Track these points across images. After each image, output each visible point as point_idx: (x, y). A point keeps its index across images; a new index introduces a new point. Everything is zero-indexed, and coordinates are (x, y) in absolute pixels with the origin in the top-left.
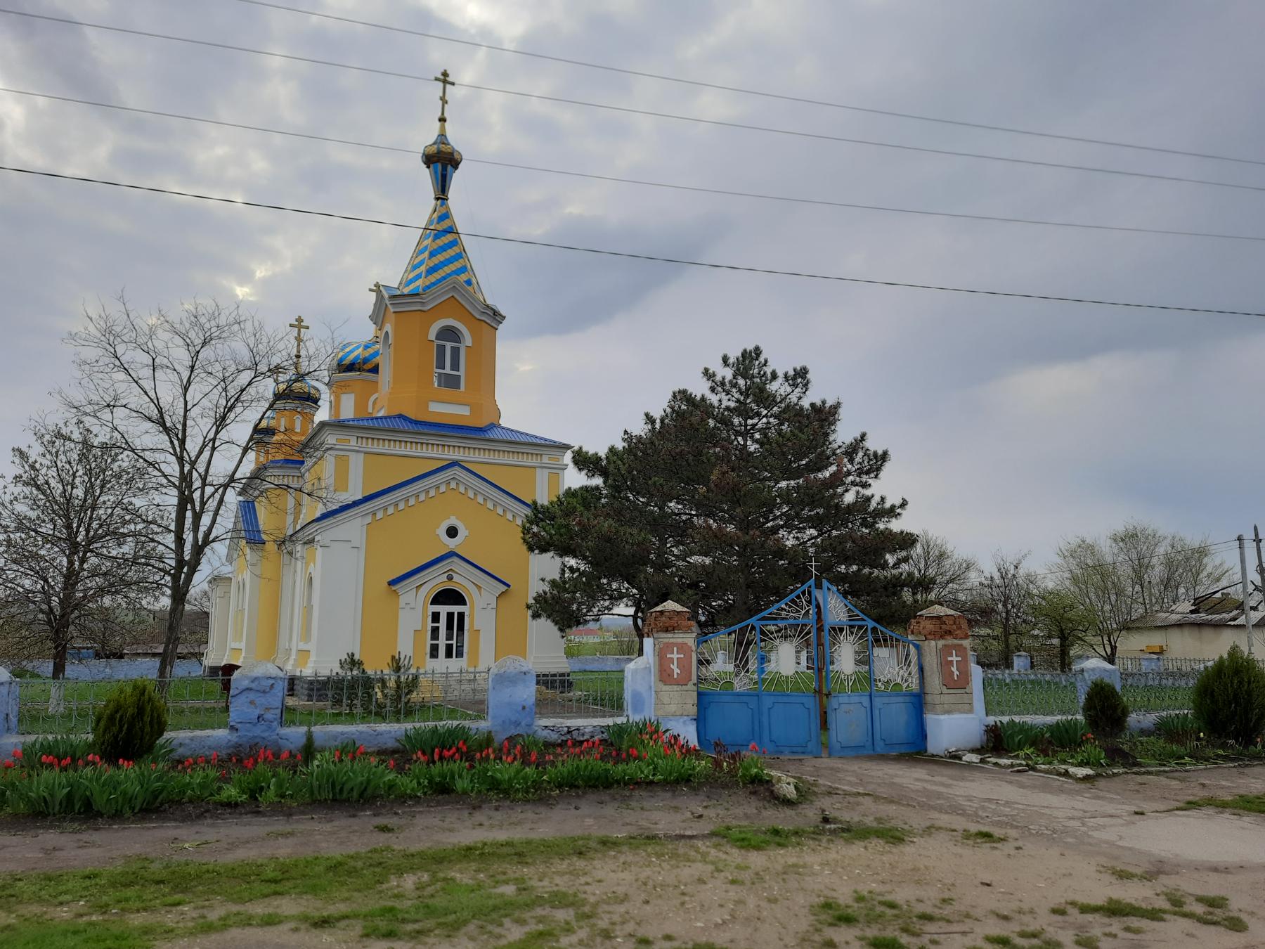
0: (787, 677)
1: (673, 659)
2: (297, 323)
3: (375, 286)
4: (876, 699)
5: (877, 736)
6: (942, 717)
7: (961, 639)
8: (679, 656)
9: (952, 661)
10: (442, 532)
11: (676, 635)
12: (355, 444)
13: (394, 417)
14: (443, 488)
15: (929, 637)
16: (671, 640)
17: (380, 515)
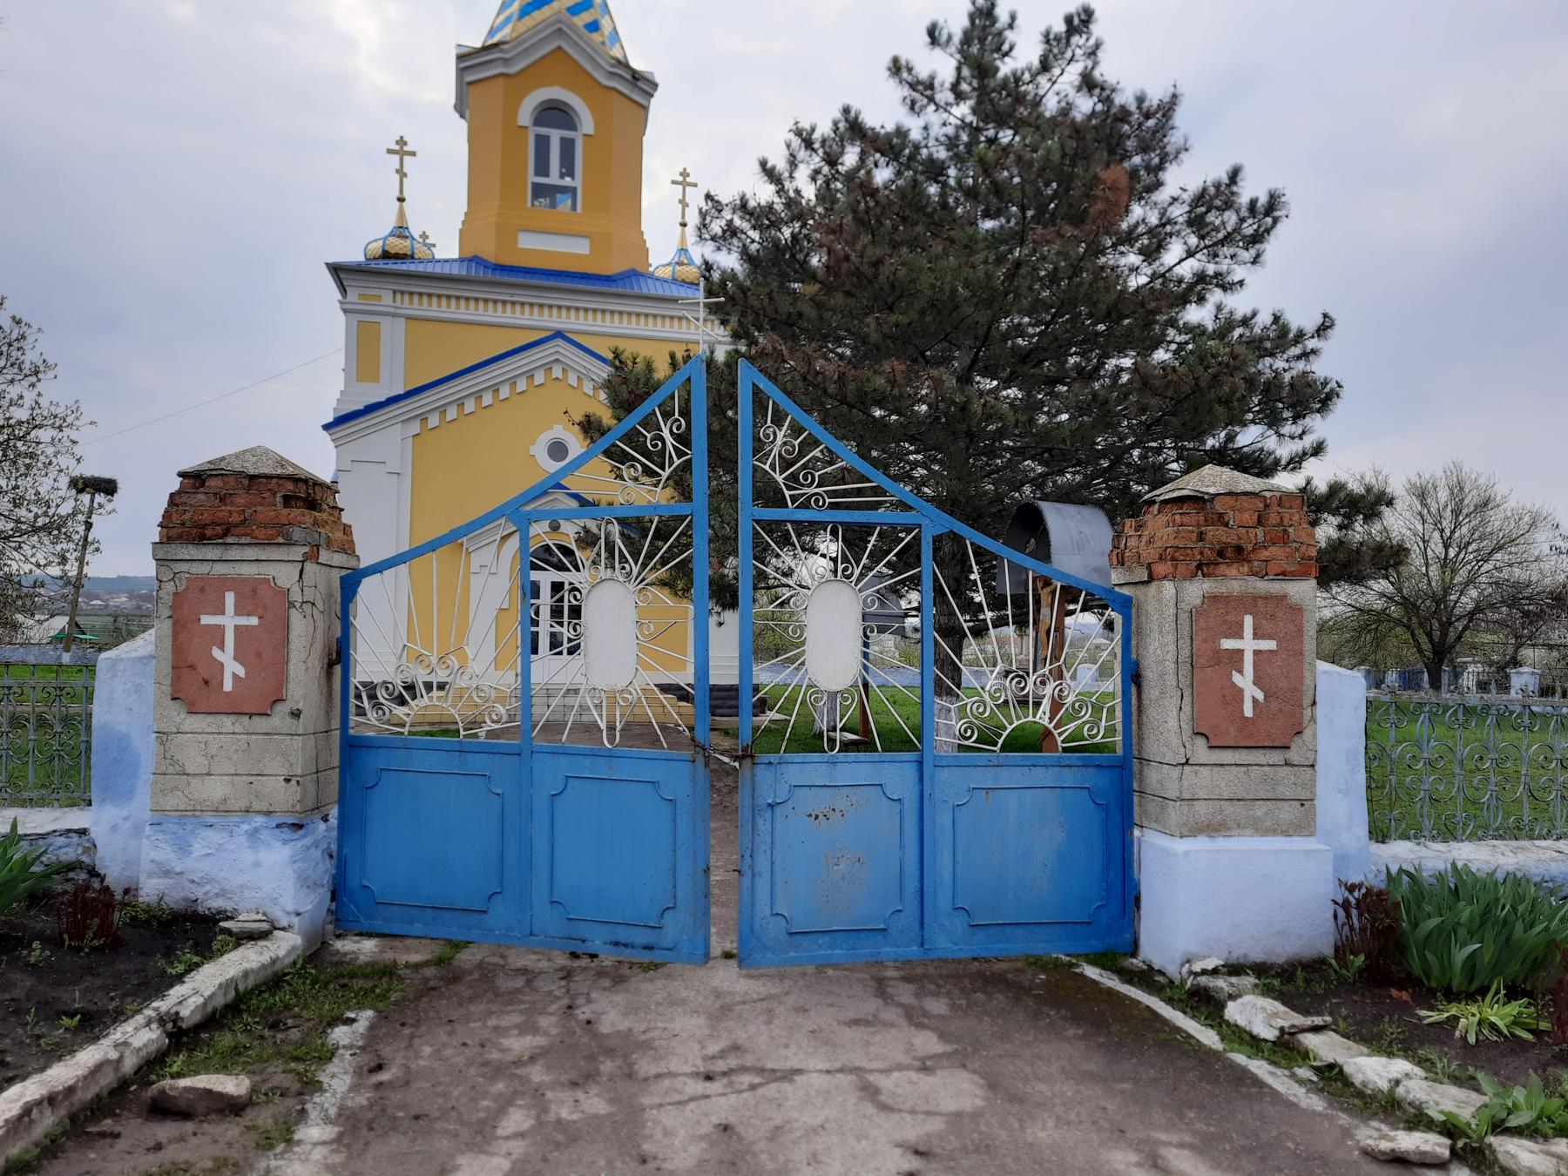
0: (833, 696)
1: (220, 630)
3: (681, 174)
4: (943, 775)
5: (941, 899)
6: (1181, 846)
7: (1284, 575)
8: (244, 621)
9: (1240, 652)
11: (234, 554)
12: (391, 303)
13: (470, 260)
14: (539, 378)
15: (1160, 569)
16: (220, 569)
17: (434, 421)
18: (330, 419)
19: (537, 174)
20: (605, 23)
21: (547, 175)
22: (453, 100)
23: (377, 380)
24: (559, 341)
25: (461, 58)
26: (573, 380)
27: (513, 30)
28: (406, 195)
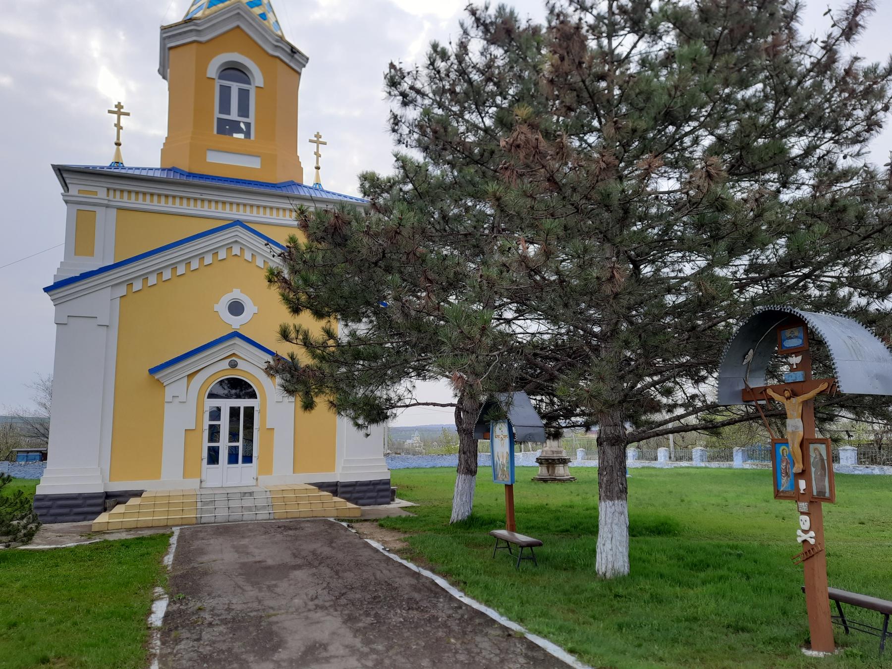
10: (222, 307)
13: (169, 170)
14: (222, 254)
17: (138, 285)
18: (51, 283)
19: (220, 112)
20: (270, 15)
21: (229, 114)
23: (92, 254)
24: (239, 228)
25: (164, 29)
26: (248, 256)
27: (203, 13)
28: (121, 141)
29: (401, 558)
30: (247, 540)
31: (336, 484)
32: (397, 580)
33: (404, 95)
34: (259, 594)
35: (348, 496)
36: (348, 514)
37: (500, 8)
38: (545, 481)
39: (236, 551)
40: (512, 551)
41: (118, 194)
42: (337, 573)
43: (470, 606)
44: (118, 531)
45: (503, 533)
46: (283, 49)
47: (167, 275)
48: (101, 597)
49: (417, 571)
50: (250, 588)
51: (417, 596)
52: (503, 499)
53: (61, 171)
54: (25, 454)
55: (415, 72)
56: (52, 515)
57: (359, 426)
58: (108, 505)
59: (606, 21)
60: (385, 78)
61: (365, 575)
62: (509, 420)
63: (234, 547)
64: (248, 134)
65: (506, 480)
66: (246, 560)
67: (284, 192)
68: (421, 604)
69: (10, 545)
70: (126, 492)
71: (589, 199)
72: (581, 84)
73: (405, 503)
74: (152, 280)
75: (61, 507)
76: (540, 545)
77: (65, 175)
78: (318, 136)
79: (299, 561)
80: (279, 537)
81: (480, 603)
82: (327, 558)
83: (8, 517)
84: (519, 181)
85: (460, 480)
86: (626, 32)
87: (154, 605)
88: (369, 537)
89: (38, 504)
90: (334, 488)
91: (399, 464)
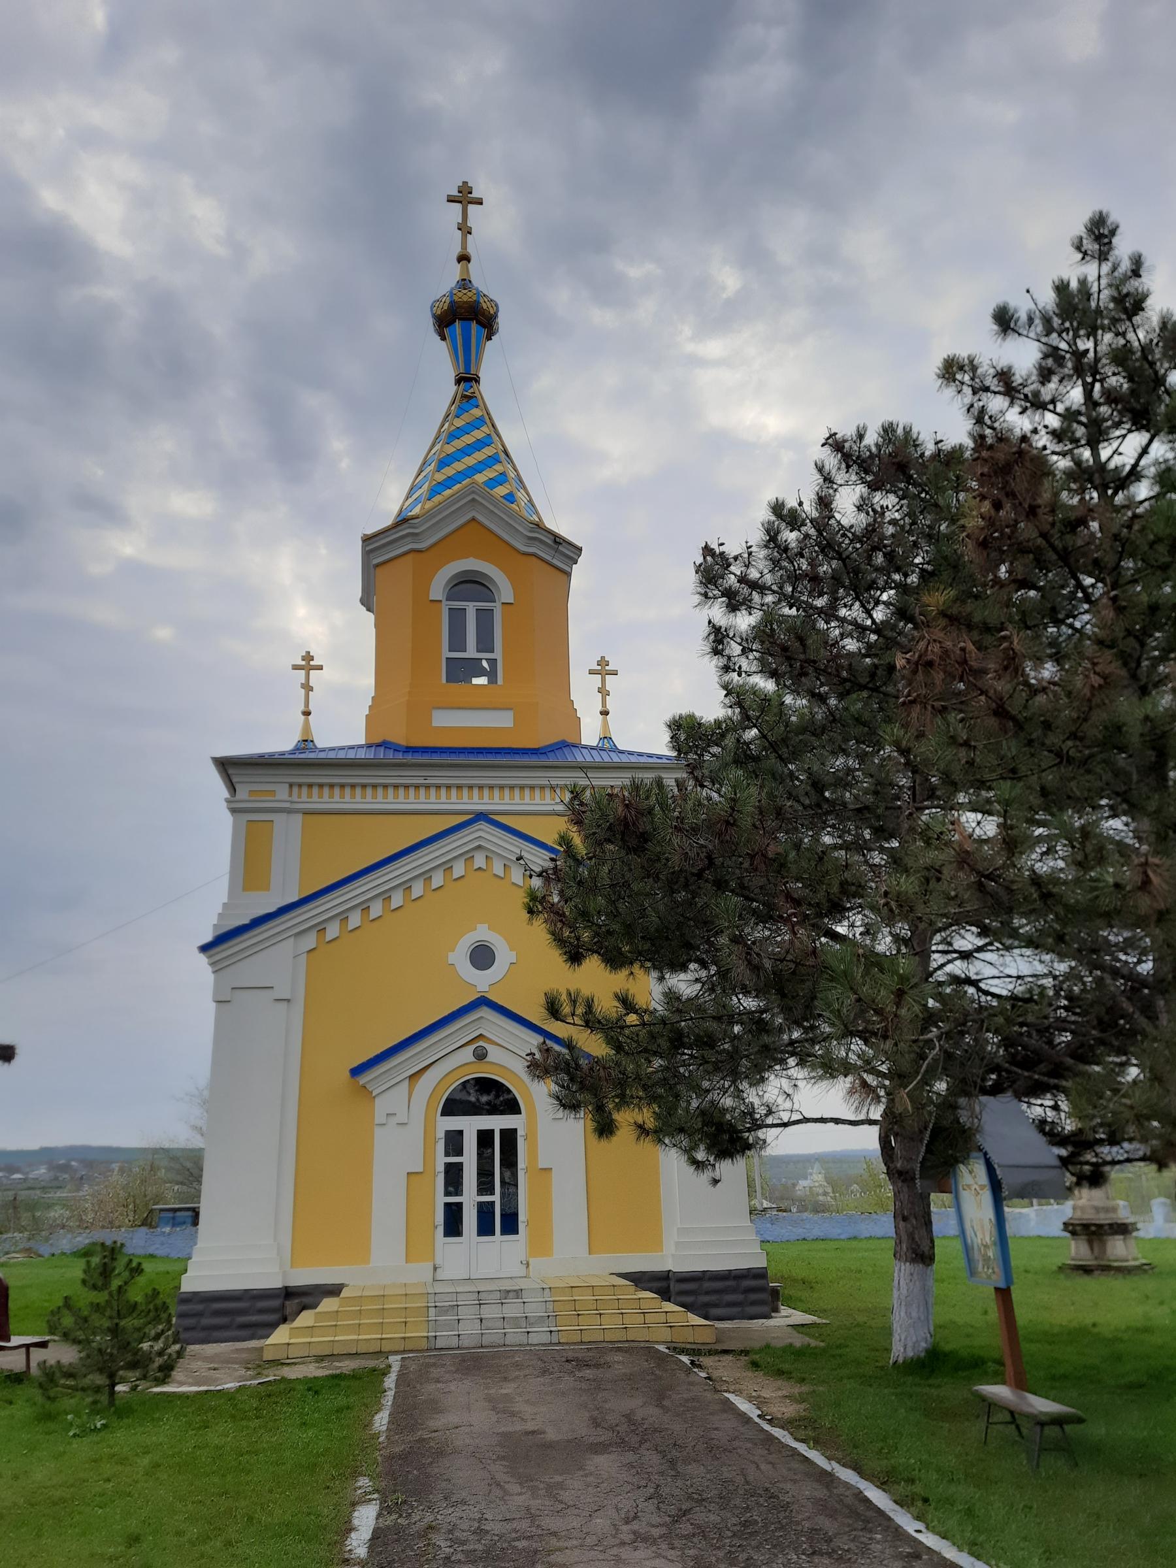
2: (303, 663)
10: (460, 957)
13: (379, 745)
17: (333, 931)
20: (520, 495)
22: (358, 593)
23: (267, 888)
24: (483, 825)
25: (367, 540)
26: (498, 869)
27: (423, 508)
29: (796, 1439)
30: (513, 1385)
31: (666, 1276)
32: (788, 1486)
33: (729, 594)
34: (531, 1502)
35: (689, 1299)
36: (690, 1337)
37: (885, 430)
38: (1086, 1270)
39: (494, 1408)
40: (1025, 1431)
41: (305, 790)
42: (673, 1463)
43: (938, 1554)
44: (303, 1360)
45: (1000, 1391)
46: (541, 541)
47: (376, 909)
48: (271, 1491)
49: (829, 1468)
50: (516, 1488)
51: (826, 1524)
52: (994, 1315)
53: (227, 766)
54: (171, 1215)
55: (746, 555)
56: (204, 1329)
57: (698, 1165)
58: (288, 1311)
59: (1083, 419)
60: (697, 573)
61: (727, 1474)
62: (985, 1154)
63: (489, 1399)
64: (492, 675)
65: (994, 1277)
66: (510, 1429)
67: (551, 760)
68: (837, 1542)
69: (137, 1386)
70: (317, 1286)
71: (1081, 739)
72: (1040, 541)
73: (799, 1317)
74: (355, 920)
75: (218, 1313)
76: (1080, 1420)
77: (230, 771)
78: (603, 662)
79: (605, 1436)
80: (568, 1382)
81: (960, 1550)
82: (655, 1430)
83: (136, 1335)
84: (939, 720)
85: (902, 1273)
86: (1124, 432)
87: (356, 1514)
88: (732, 1388)
89: (184, 1308)
90: (663, 1284)
91: (783, 1230)
